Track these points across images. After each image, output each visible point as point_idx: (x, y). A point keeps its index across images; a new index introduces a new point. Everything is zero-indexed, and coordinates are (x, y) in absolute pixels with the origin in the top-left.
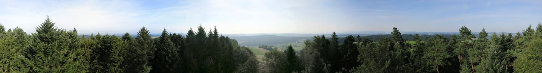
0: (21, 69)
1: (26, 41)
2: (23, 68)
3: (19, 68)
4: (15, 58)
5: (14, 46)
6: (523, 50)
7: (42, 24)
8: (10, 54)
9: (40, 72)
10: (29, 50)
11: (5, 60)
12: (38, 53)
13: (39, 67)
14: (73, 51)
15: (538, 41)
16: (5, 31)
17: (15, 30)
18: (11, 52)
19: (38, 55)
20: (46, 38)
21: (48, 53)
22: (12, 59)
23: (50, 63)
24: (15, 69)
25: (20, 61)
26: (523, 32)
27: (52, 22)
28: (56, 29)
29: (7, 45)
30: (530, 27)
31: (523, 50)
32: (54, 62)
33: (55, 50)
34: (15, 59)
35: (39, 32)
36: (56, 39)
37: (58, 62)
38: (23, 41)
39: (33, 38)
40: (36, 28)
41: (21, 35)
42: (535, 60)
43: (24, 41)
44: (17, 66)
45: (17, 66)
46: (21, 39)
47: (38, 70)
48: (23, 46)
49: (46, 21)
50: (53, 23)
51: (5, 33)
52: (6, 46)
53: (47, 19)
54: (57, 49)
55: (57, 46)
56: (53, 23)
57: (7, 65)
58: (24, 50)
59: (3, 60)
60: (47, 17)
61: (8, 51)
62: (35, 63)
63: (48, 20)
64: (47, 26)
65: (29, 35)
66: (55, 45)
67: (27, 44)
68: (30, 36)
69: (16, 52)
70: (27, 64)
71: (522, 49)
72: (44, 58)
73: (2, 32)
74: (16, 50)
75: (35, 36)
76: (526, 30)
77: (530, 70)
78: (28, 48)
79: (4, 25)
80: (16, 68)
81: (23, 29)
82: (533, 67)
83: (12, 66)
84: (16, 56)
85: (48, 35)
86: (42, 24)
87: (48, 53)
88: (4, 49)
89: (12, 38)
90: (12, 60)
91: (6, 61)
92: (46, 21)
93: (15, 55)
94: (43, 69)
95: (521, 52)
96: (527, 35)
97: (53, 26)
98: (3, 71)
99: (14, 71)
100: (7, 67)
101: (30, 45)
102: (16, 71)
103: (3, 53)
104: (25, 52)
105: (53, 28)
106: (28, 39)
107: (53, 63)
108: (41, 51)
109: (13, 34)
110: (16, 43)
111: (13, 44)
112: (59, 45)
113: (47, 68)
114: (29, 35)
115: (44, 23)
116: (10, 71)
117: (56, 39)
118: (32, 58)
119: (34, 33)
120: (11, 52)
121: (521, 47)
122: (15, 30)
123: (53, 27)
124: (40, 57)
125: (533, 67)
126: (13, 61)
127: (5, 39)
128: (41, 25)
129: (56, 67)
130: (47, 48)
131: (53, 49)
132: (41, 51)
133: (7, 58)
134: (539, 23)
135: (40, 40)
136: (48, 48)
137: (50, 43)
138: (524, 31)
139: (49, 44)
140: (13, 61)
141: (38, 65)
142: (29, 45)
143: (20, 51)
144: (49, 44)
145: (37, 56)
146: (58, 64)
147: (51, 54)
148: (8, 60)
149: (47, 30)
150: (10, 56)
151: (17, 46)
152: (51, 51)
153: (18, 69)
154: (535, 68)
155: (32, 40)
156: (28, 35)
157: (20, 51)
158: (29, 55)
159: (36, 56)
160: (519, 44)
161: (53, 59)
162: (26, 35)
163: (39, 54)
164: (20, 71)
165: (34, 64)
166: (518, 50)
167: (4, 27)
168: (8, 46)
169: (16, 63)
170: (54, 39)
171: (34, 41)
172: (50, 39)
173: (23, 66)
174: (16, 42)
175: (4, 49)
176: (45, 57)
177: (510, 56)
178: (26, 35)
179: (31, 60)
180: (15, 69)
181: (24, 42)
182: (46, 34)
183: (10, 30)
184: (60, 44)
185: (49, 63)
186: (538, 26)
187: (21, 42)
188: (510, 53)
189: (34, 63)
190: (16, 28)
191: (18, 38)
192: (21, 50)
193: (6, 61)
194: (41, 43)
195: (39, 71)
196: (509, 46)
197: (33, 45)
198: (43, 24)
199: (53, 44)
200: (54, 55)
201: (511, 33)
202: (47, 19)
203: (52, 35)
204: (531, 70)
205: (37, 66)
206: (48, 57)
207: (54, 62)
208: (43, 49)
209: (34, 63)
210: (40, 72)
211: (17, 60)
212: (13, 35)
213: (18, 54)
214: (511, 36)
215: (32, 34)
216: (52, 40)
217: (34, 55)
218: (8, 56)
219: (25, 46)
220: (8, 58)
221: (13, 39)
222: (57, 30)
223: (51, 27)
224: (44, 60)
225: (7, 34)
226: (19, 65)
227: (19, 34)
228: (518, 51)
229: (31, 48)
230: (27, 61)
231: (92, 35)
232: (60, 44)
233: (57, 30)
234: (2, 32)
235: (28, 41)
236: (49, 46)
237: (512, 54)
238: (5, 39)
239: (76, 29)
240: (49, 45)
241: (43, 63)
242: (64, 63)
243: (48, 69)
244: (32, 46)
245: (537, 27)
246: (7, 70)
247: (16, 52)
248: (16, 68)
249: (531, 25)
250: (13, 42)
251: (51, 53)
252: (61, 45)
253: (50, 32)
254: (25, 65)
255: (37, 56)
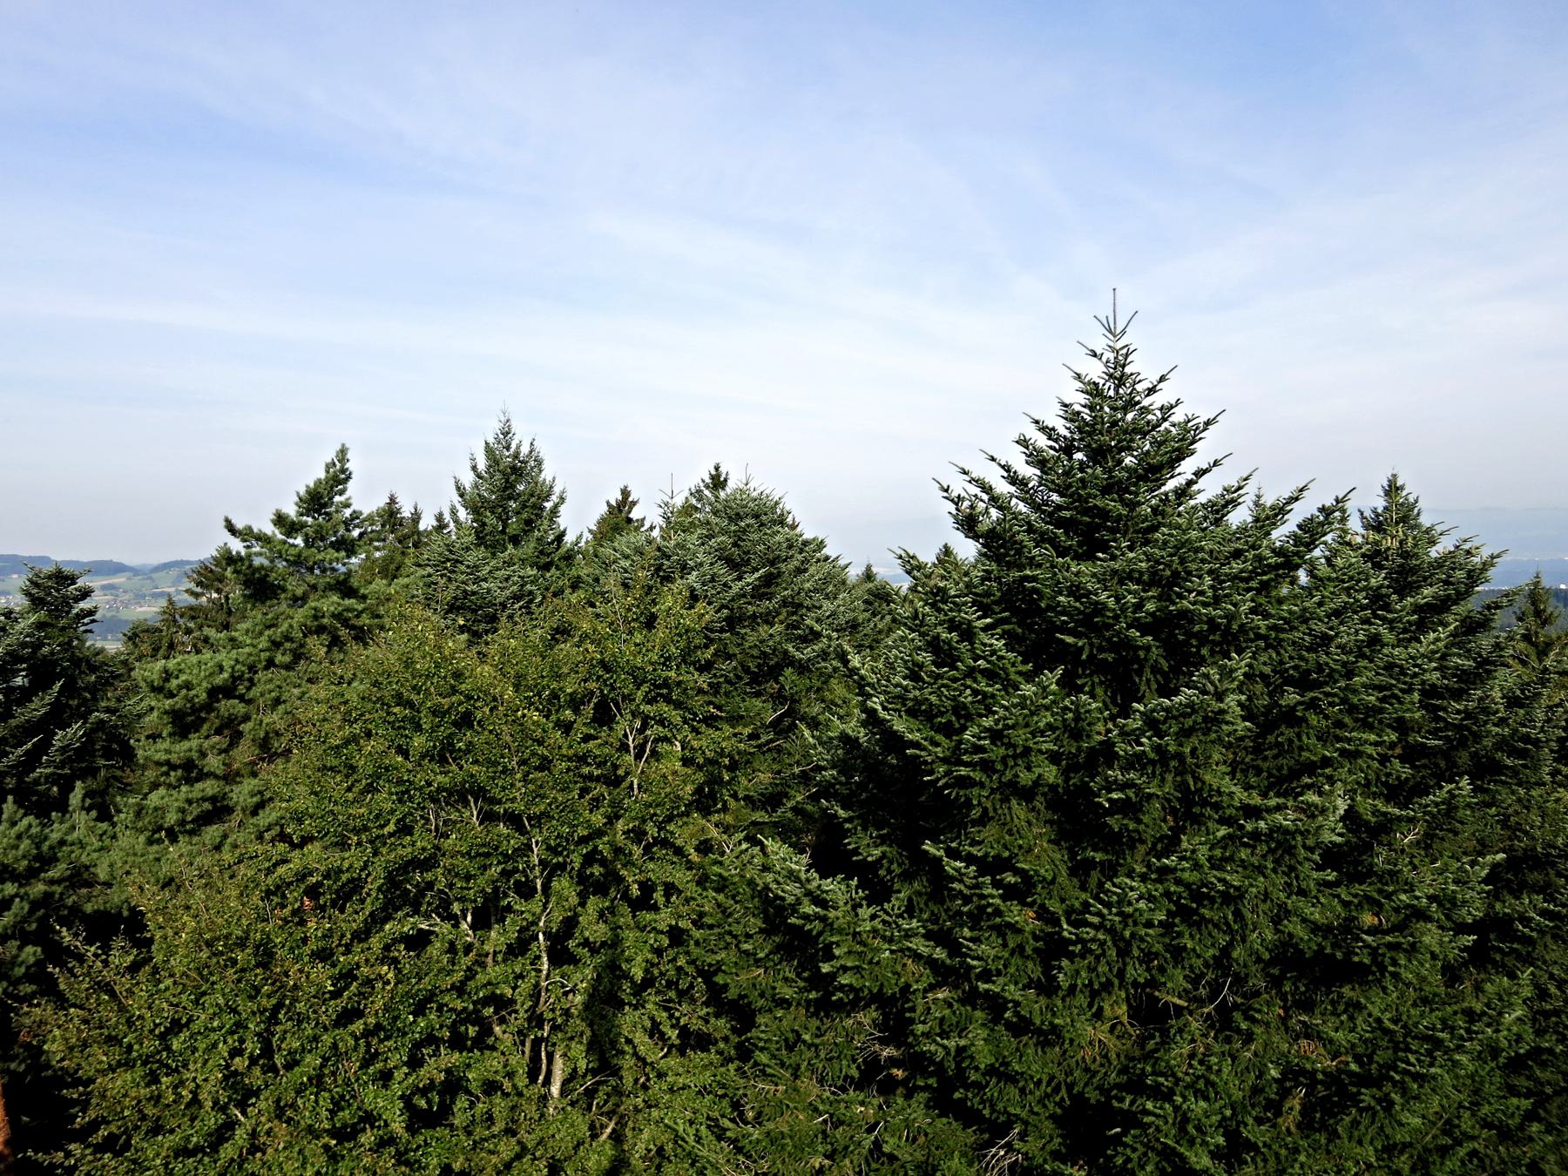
0: (766, 1027)
1: (824, 655)
2: (791, 1019)
3: (742, 1014)
4: (681, 877)
5: (675, 716)
6: (242, 793)
7: (1042, 441)
8: (620, 825)
9: (1012, 1079)
10: (872, 767)
11: (558, 916)
12: (983, 820)
13: (995, 1005)
14: (1450, 806)
15: (408, 663)
16: (563, 521)
17: (681, 519)
18: (635, 802)
19: (989, 841)
20: (1091, 619)
21: (1114, 822)
22: (647, 888)
23: (1148, 958)
24: (684, 1032)
25: (755, 923)
26: (237, 546)
27: (1167, 410)
28: (1234, 503)
29: (588, 710)
30: (338, 477)
31: (242, 793)
32: (1201, 947)
33: (1217, 778)
34: (692, 890)
35: (996, 543)
36: (1229, 638)
37: (1262, 936)
38: (788, 660)
39: (916, 618)
40: (959, 486)
41: (769, 580)
42: (376, 921)
43: (809, 652)
44: (715, 995)
45: (715, 995)
46: (764, 630)
47: (985, 1059)
48: (782, 728)
49: (1094, 390)
50: (1178, 416)
51: (553, 555)
52: (567, 728)
53: (1095, 371)
54: (1234, 768)
55: (1243, 726)
56: (1178, 416)
57: (582, 978)
58: (805, 778)
59: (535, 905)
60: (1100, 343)
61: (599, 789)
62: (940, 954)
63: (1120, 381)
64: (1098, 455)
65: (869, 576)
66: (1217, 719)
67: (838, 689)
68: (880, 596)
69: (705, 802)
70: (841, 963)
71: (230, 777)
72: (1063, 878)
73: (515, 540)
74: (700, 777)
75: (938, 597)
76: (280, 520)
77: (301, 1074)
78: (845, 739)
79: (544, 451)
80: (693, 1015)
81: (788, 504)
82: (346, 1017)
83: (648, 982)
84: (705, 847)
85: (1124, 577)
86: (1042, 441)
87: (1114, 822)
88: (545, 765)
89: (650, 622)
90: (644, 902)
91: (570, 924)
92: (1094, 390)
93: (684, 834)
94: (1049, 1037)
95: (212, 832)
96: (295, 586)
97: (1182, 453)
98: (533, 1075)
99: (674, 1062)
100: (587, 1006)
101: (875, 703)
102: (698, 1057)
103: (538, 820)
104: (814, 798)
105: (1183, 493)
106: (854, 626)
107: (1178, 953)
108: (1027, 794)
109: (665, 568)
110: (703, 681)
111: (662, 691)
112: (1268, 721)
113: (1101, 1033)
114: (869, 576)
115: (1062, 428)
116: (628, 1062)
117: (1229, 638)
118: (907, 877)
119: (928, 557)
120: (635, 802)
121: (214, 762)
122: (688, 509)
123: (1187, 467)
124: (1003, 864)
125: (346, 1017)
126: (664, 919)
127: (562, 632)
128: (1023, 442)
129: (1222, 1023)
130: (1106, 753)
131: (1180, 772)
132: (1027, 794)
133: (582, 879)
134: (490, 435)
135: (1012, 641)
136: (1121, 748)
137: (1146, 681)
138: (246, 534)
139: (1123, 696)
140: (664, 919)
141: (986, 976)
142: (871, 713)
143: (744, 785)
144: (1123, 696)
145: (970, 859)
146: (1257, 981)
147: (1150, 833)
148: (594, 904)
149: (1104, 514)
150: (618, 851)
151: (710, 721)
152: (1161, 788)
153: (721, 1026)
154: (368, 1033)
155: (901, 645)
156: (854, 573)
157: (744, 785)
158: (868, 847)
159: (953, 854)
160: (183, 723)
161: (1184, 913)
162: (826, 580)
163: (989, 833)
164: (744, 1053)
165: (931, 963)
166: (169, 802)
167: (547, 475)
168: (604, 717)
169: (705, 949)
170: (1202, 639)
171: (926, 657)
172: (1144, 629)
173: (787, 992)
174: (705, 668)
175: (545, 765)
176: (1080, 870)
177: (35, 905)
178: (834, 580)
179: (897, 903)
180: (684, 1032)
181: (802, 668)
182: (1085, 571)
183: (619, 517)
184: (1291, 697)
185: (1124, 953)
186: (482, 465)
187: (764, 671)
188: (45, 860)
189: (921, 946)
190: (698, 494)
191: (732, 623)
192: (765, 777)
193: (570, 924)
194: (1028, 689)
195: (991, 1071)
196: (32, 759)
197: (912, 713)
198: (1049, 432)
199: (1186, 695)
200: (1194, 843)
201: (63, 554)
202: (1095, 371)
203: (1166, 582)
204: (317, 1081)
205: (971, 998)
206: (1110, 871)
207: (1201, 947)
208: (1054, 758)
209: (921, 946)
210: (1012, 1079)
211: (709, 901)
212: (667, 579)
213: (727, 829)
214: (67, 603)
215: (911, 565)
216: (1173, 649)
217: (928, 847)
218: (589, 860)
219: (814, 724)
220: (588, 887)
221: (660, 633)
222: (1239, 517)
223: (1154, 471)
224: (1055, 906)
225: (584, 570)
226: (740, 981)
227: (737, 565)
228: (172, 818)
229: (893, 741)
230: (837, 915)
231: (1537, 584)
232: (1291, 697)
233: (1239, 517)
234: (515, 540)
235: (855, 661)
236: (1135, 723)
237: (80, 877)
238: (562, 632)
239: (1412, 488)
240: (1126, 712)
241: (1053, 949)
242: (1357, 974)
243: (1112, 1043)
244: (899, 726)
245: (468, 479)
246: (578, 1050)
247: (705, 802)
248: (693, 1015)
249: (343, 453)
250: (666, 661)
251: (1154, 822)
252: (1290, 717)
253: (1145, 536)
254: (823, 983)
255: (95, 851)
